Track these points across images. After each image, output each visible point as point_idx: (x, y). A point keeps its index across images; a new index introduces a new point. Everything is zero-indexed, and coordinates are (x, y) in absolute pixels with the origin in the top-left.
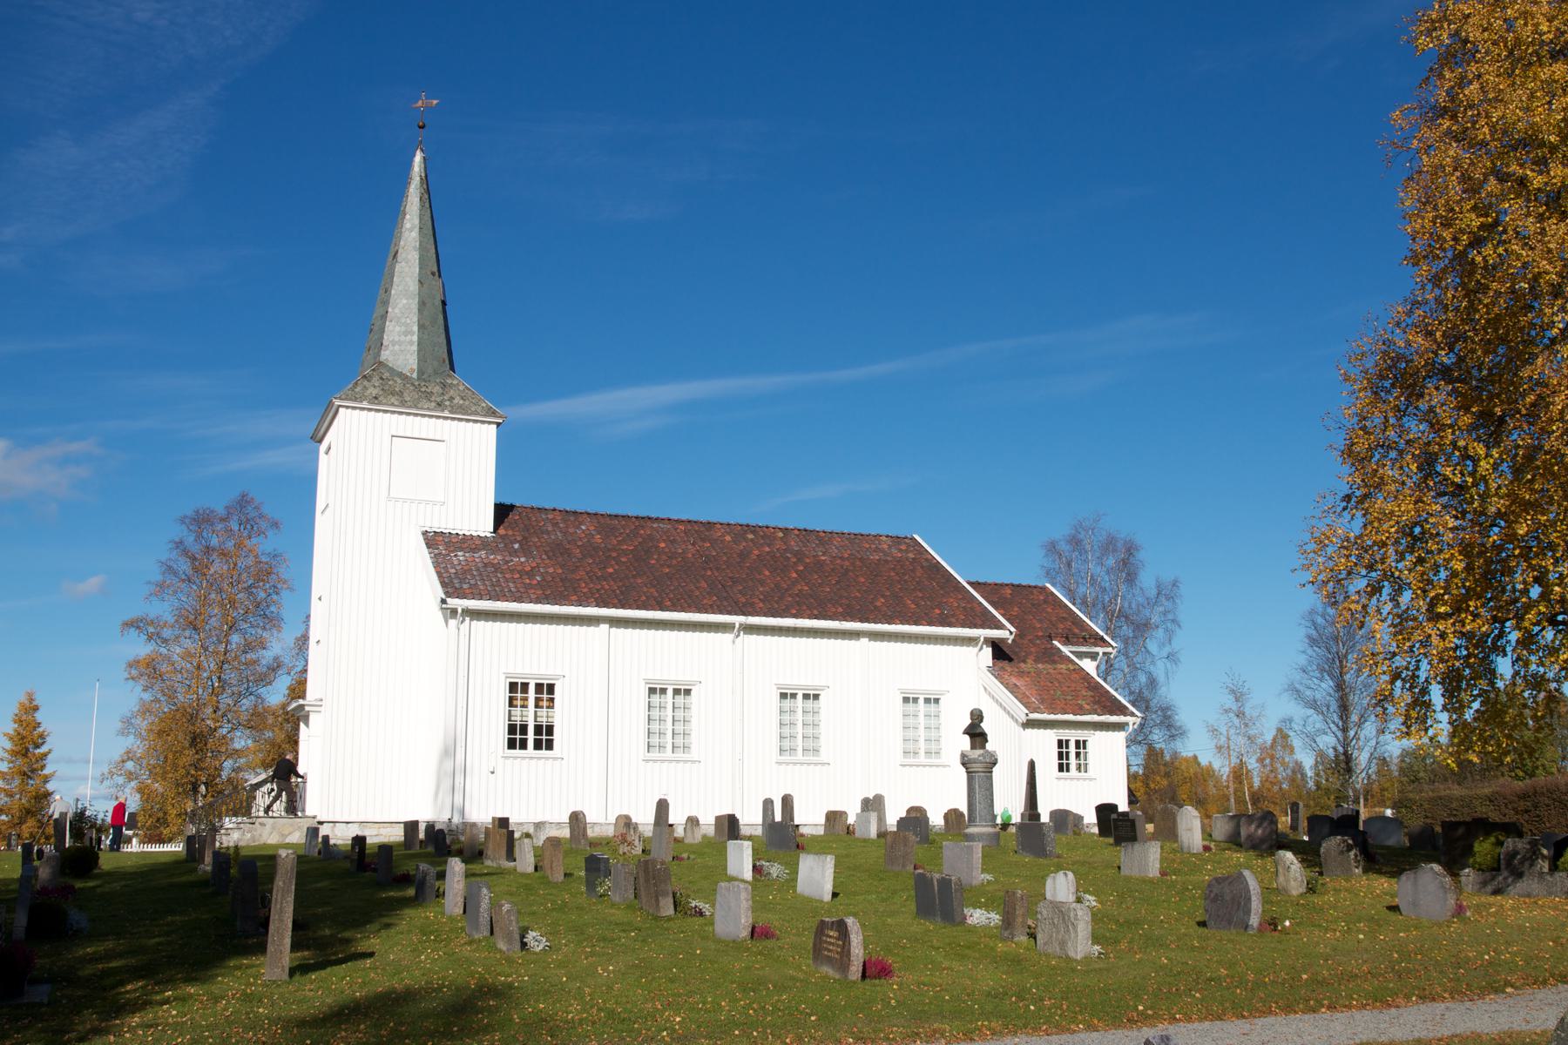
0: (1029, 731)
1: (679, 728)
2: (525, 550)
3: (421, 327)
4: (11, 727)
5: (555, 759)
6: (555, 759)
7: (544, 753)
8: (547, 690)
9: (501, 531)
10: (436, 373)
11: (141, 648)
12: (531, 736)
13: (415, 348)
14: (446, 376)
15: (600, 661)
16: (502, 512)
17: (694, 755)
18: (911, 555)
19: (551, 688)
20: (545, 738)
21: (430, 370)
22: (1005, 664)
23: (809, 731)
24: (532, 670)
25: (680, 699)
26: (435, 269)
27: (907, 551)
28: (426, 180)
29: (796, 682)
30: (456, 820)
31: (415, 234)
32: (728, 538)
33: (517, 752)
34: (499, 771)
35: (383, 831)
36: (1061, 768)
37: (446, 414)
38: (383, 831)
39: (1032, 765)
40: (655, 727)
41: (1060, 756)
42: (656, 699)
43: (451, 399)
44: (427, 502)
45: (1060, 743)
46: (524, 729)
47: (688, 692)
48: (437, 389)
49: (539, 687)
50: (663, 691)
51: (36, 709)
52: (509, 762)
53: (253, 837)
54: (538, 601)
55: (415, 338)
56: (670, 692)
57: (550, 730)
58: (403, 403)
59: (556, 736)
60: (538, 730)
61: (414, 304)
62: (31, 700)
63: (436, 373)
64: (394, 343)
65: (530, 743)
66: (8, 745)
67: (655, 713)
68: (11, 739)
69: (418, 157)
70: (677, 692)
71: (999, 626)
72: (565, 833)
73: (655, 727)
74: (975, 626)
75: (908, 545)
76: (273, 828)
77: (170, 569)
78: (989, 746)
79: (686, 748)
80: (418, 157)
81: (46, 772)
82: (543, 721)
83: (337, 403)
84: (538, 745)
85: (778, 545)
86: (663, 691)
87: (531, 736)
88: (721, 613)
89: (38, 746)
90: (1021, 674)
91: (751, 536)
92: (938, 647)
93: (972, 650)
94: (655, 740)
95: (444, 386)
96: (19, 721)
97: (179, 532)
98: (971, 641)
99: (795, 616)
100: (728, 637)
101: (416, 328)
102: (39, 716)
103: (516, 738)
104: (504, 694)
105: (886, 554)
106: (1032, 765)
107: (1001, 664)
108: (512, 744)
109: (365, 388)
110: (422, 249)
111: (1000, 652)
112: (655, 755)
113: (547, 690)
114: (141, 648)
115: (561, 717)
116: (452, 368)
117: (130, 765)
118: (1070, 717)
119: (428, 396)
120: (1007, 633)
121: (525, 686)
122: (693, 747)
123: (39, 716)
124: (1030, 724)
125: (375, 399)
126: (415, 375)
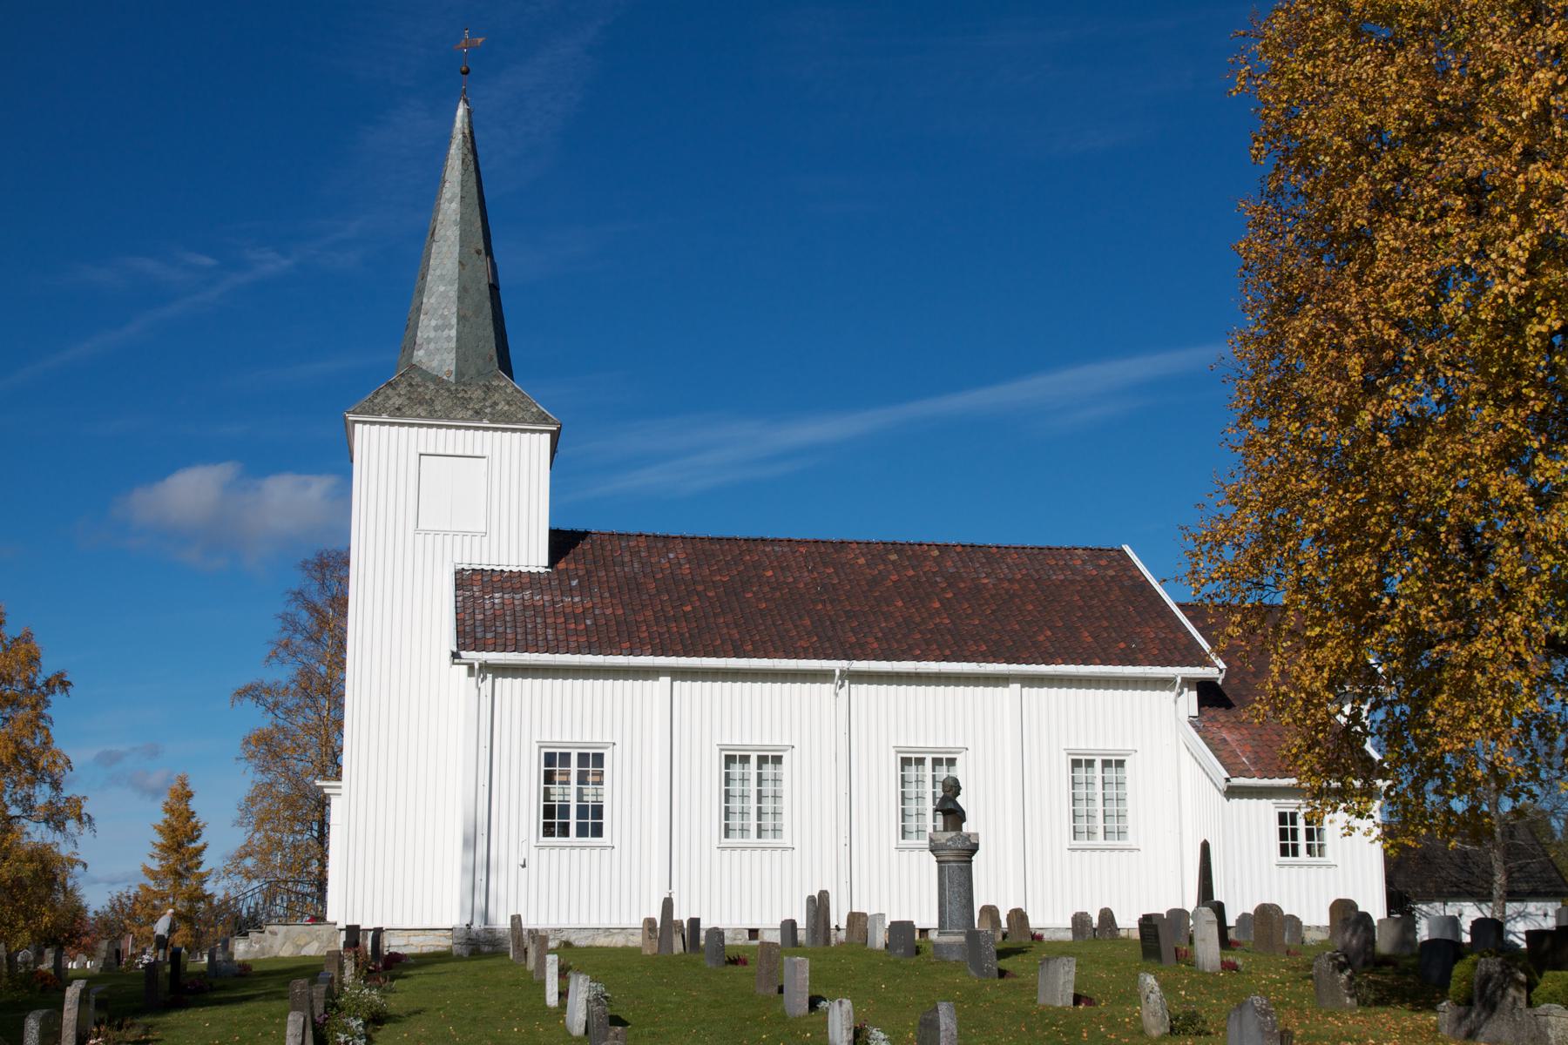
0: (1235, 802)
1: (1112, 808)
2: (583, 589)
3: (462, 318)
4: (160, 817)
5: (603, 847)
6: (603, 847)
7: (590, 840)
8: (593, 761)
9: (561, 565)
10: (479, 374)
11: (257, 718)
12: (573, 821)
13: (453, 344)
14: (495, 375)
15: (659, 725)
16: (562, 542)
17: (786, 840)
18: (1111, 573)
19: (599, 759)
20: (592, 822)
21: (473, 371)
22: (1221, 714)
23: (1112, 808)
24: (573, 735)
25: (1111, 773)
26: (481, 246)
27: (1107, 567)
28: (471, 139)
29: (747, 741)
30: (478, 925)
31: (455, 205)
32: (862, 561)
33: (1290, 859)
34: (532, 864)
35: (413, 940)
36: (1284, 851)
37: (486, 424)
38: (413, 940)
39: (1205, 848)
40: (1082, 808)
41: (1283, 834)
42: (1081, 773)
43: (495, 404)
44: (465, 533)
45: (1282, 818)
46: (565, 811)
47: (1120, 764)
48: (479, 393)
49: (583, 758)
50: (1090, 763)
51: (190, 795)
52: (545, 852)
53: (262, 948)
54: (578, 651)
55: (453, 333)
56: (1098, 765)
57: (598, 811)
58: (431, 415)
59: (606, 821)
60: (582, 812)
61: (453, 292)
62: (184, 785)
63: (479, 374)
64: (429, 340)
65: (573, 829)
66: (159, 839)
67: (1082, 791)
68: (161, 831)
69: (461, 111)
70: (1106, 764)
71: (1204, 662)
72: (775, 938)
73: (1082, 808)
74: (1170, 664)
75: (1113, 559)
76: (286, 937)
77: (290, 623)
78: (967, 827)
79: (1121, 833)
80: (461, 111)
81: (203, 869)
82: (590, 799)
83: (351, 418)
84: (582, 831)
85: (930, 566)
86: (1090, 763)
87: (573, 821)
88: (816, 657)
89: (193, 840)
90: (1238, 725)
91: (894, 557)
92: (1119, 693)
93: (1168, 696)
94: (1082, 824)
95: (488, 389)
96: (170, 810)
97: (298, 580)
98: (1165, 684)
99: (917, 659)
100: (828, 688)
101: (454, 321)
102: (194, 804)
103: (553, 821)
104: (536, 769)
105: (1074, 571)
106: (1205, 848)
107: (1211, 712)
108: (548, 831)
109: (388, 398)
110: (464, 222)
111: (1209, 694)
112: (1083, 842)
113: (593, 761)
114: (257, 718)
115: (613, 795)
116: (506, 365)
117: (249, 862)
118: (1277, 782)
119: (465, 403)
120: (1215, 671)
121: (565, 758)
122: (1130, 831)
123: (194, 804)
124: (1232, 792)
125: (398, 411)
126: (452, 379)
